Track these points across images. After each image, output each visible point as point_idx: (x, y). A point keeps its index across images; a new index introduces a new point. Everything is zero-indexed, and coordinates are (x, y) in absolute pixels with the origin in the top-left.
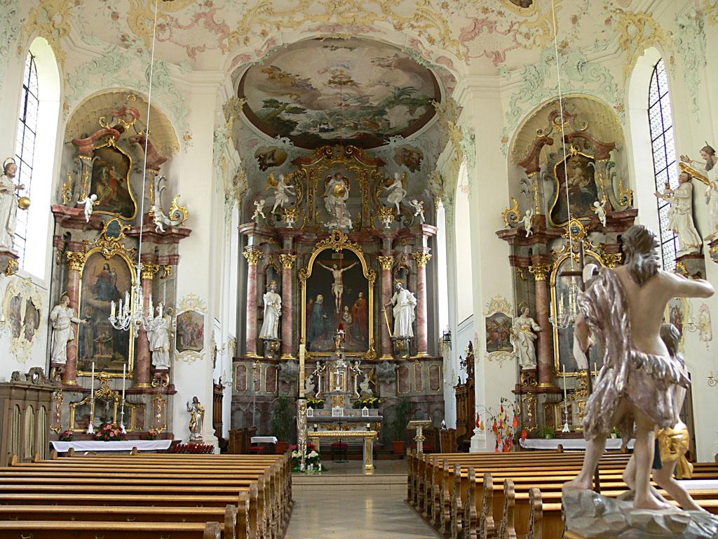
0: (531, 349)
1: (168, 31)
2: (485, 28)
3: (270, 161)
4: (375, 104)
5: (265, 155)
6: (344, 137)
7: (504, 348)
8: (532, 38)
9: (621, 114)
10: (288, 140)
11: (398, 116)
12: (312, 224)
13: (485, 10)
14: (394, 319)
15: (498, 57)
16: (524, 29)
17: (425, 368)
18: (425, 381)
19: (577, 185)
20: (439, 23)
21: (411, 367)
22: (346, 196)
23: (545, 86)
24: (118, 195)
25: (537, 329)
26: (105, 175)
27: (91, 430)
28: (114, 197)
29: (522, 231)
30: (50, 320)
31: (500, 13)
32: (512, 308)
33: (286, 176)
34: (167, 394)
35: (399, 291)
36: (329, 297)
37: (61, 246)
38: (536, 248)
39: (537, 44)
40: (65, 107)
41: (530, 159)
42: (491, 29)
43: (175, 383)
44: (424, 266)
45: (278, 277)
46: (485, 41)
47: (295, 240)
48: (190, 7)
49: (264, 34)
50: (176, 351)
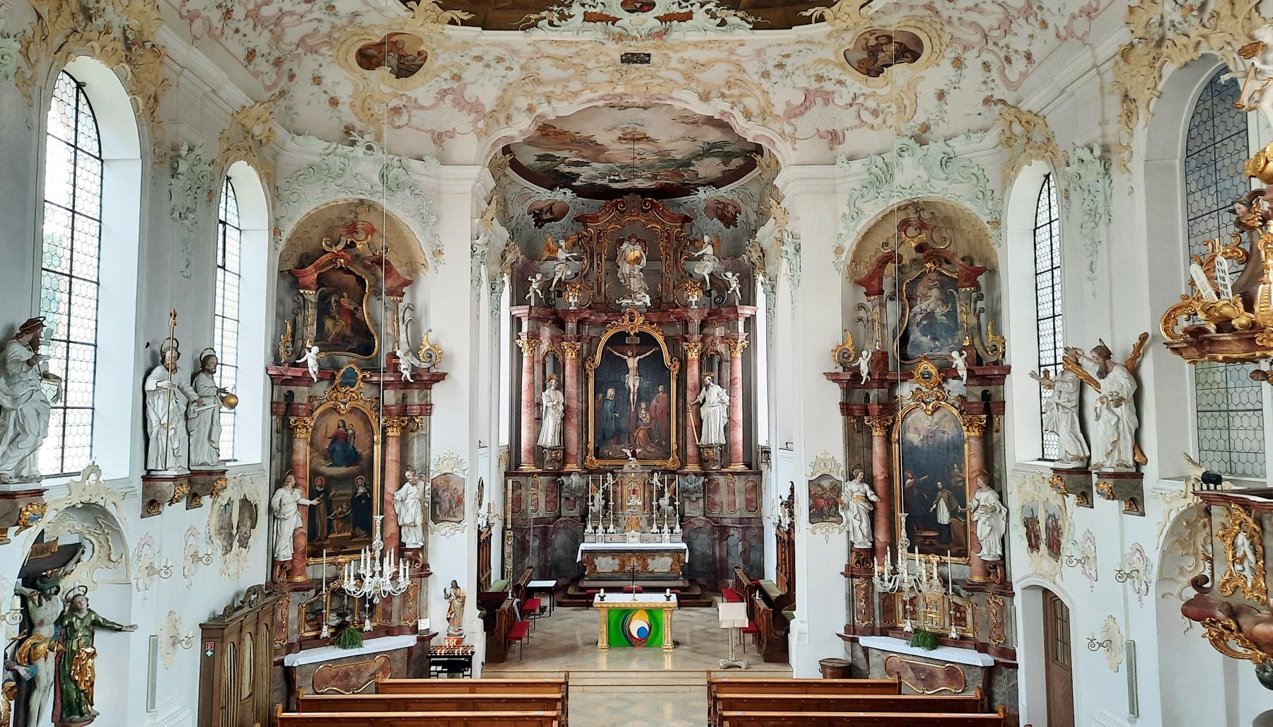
0: (865, 525)
1: (405, 117)
2: (819, 101)
3: (549, 216)
4: (678, 157)
5: (541, 210)
6: (640, 186)
7: (831, 519)
8: (881, 116)
9: (995, 232)
10: (569, 192)
11: (710, 168)
12: (601, 299)
13: (820, 78)
14: (701, 421)
15: (835, 138)
16: (871, 104)
17: (739, 483)
18: (740, 500)
19: (932, 312)
20: (757, 93)
21: (721, 480)
22: (644, 261)
23: (895, 183)
24: (352, 328)
25: (873, 498)
26: (334, 305)
27: (325, 632)
28: (348, 332)
29: (856, 375)
30: (270, 509)
31: (840, 82)
32: (842, 468)
33: (566, 239)
34: (421, 576)
35: (707, 387)
36: (621, 388)
37: (282, 410)
38: (873, 393)
39: (889, 123)
40: (276, 232)
41: (871, 277)
42: (827, 102)
43: (430, 561)
44: (739, 355)
45: (559, 368)
46: (819, 118)
47: (581, 323)
48: (433, 82)
49: (530, 109)
50: (431, 523)
